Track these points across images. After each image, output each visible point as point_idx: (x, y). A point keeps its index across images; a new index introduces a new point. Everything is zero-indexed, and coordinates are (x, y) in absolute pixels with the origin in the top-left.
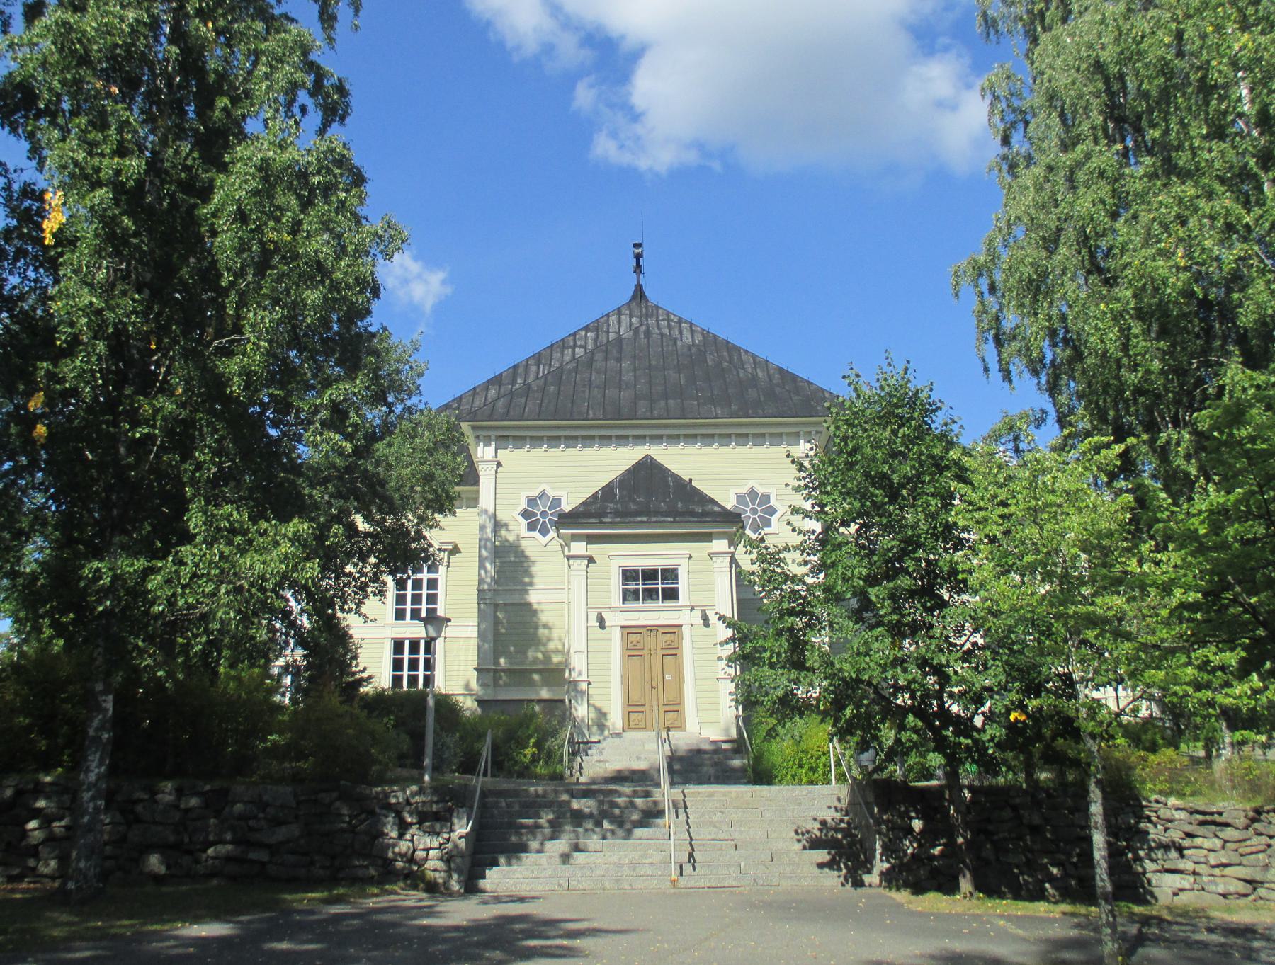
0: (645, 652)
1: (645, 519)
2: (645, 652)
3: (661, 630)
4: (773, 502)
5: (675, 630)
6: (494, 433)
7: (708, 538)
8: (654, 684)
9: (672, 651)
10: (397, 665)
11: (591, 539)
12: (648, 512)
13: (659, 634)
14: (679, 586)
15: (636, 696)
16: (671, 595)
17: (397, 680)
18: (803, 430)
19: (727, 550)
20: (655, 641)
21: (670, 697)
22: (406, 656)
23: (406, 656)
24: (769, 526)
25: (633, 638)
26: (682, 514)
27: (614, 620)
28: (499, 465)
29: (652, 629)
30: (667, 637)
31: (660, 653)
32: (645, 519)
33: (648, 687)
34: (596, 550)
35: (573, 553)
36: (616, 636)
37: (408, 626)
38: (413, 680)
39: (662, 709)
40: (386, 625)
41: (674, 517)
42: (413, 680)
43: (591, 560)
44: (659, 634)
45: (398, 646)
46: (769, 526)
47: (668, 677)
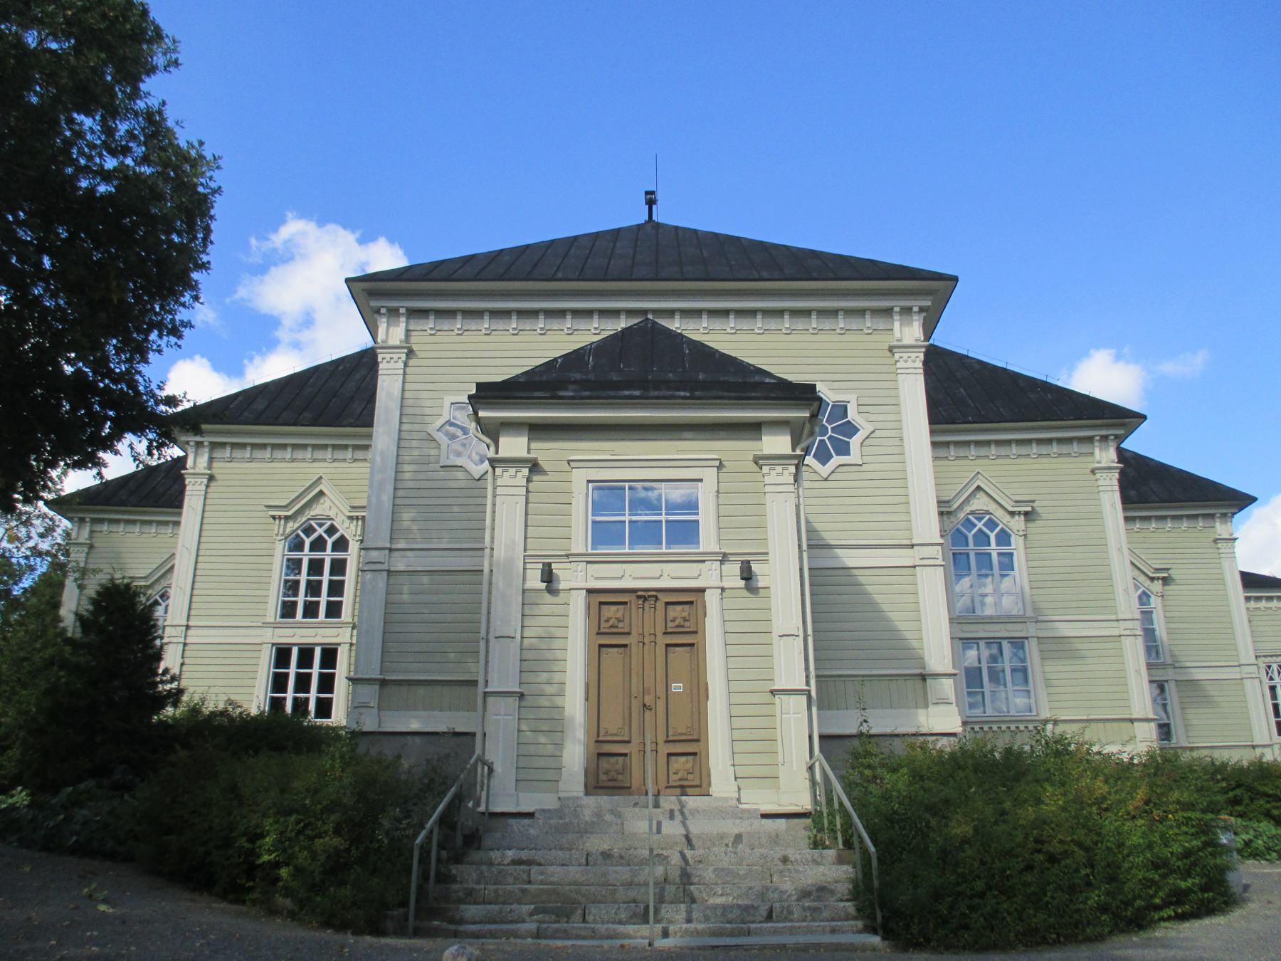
0: (631, 640)
1: (637, 393)
2: (631, 640)
3: (664, 598)
4: (852, 414)
5: (691, 598)
6: (403, 305)
7: (754, 429)
8: (648, 700)
9: (687, 639)
10: (279, 683)
11: (537, 430)
12: (648, 387)
13: (660, 605)
14: (700, 518)
15: (612, 724)
16: (686, 532)
17: (277, 704)
18: (897, 304)
19: (788, 451)
20: (654, 620)
21: (680, 725)
22: (293, 670)
23: (293, 670)
24: (847, 453)
25: (610, 612)
26: (705, 386)
27: (569, 577)
28: (410, 353)
29: (646, 596)
30: (675, 612)
31: (663, 640)
32: (637, 393)
33: (636, 705)
34: (546, 451)
35: (502, 454)
36: (578, 604)
37: (300, 626)
38: (300, 705)
39: (664, 749)
40: (266, 625)
41: (692, 390)
42: (300, 705)
43: (535, 467)
44: (660, 605)
45: (282, 655)
46: (847, 453)
47: (677, 688)
